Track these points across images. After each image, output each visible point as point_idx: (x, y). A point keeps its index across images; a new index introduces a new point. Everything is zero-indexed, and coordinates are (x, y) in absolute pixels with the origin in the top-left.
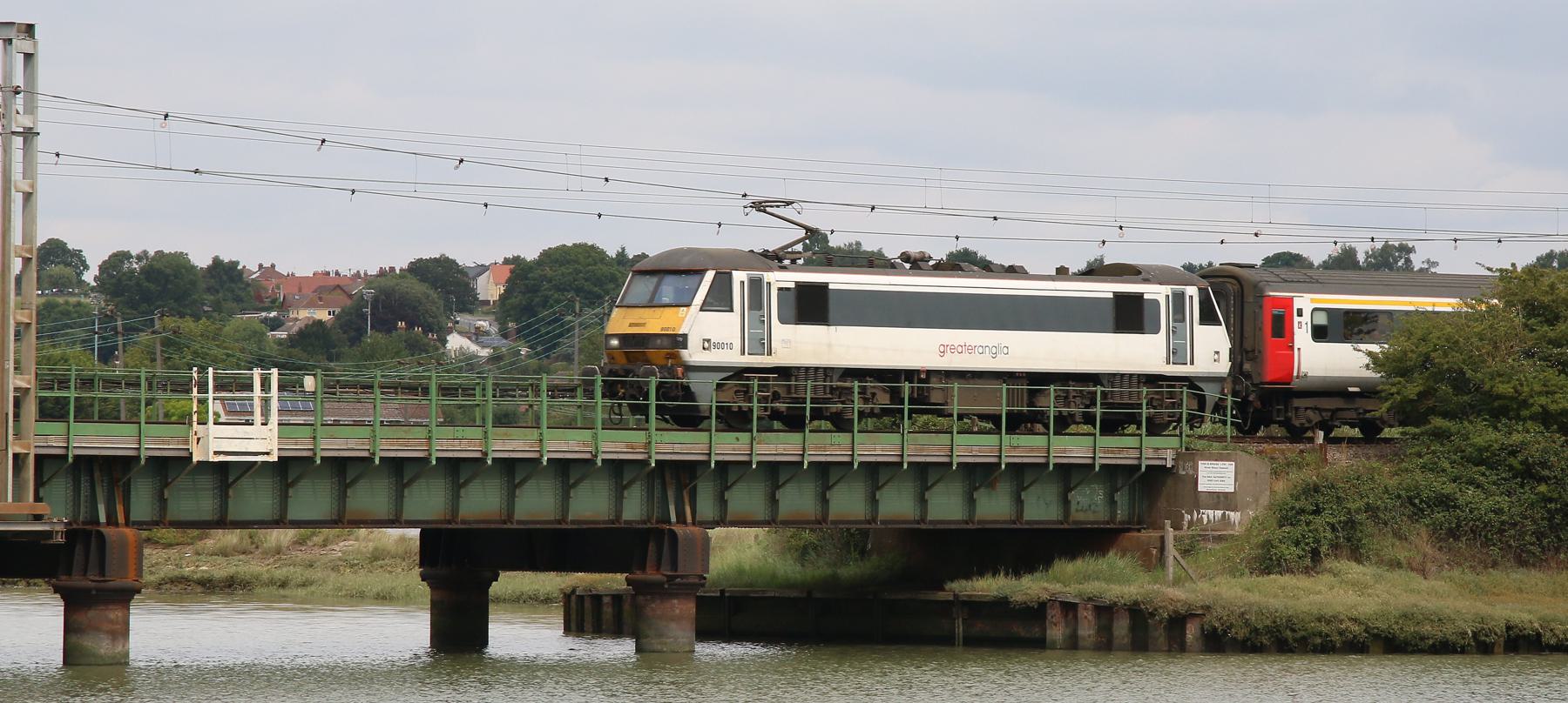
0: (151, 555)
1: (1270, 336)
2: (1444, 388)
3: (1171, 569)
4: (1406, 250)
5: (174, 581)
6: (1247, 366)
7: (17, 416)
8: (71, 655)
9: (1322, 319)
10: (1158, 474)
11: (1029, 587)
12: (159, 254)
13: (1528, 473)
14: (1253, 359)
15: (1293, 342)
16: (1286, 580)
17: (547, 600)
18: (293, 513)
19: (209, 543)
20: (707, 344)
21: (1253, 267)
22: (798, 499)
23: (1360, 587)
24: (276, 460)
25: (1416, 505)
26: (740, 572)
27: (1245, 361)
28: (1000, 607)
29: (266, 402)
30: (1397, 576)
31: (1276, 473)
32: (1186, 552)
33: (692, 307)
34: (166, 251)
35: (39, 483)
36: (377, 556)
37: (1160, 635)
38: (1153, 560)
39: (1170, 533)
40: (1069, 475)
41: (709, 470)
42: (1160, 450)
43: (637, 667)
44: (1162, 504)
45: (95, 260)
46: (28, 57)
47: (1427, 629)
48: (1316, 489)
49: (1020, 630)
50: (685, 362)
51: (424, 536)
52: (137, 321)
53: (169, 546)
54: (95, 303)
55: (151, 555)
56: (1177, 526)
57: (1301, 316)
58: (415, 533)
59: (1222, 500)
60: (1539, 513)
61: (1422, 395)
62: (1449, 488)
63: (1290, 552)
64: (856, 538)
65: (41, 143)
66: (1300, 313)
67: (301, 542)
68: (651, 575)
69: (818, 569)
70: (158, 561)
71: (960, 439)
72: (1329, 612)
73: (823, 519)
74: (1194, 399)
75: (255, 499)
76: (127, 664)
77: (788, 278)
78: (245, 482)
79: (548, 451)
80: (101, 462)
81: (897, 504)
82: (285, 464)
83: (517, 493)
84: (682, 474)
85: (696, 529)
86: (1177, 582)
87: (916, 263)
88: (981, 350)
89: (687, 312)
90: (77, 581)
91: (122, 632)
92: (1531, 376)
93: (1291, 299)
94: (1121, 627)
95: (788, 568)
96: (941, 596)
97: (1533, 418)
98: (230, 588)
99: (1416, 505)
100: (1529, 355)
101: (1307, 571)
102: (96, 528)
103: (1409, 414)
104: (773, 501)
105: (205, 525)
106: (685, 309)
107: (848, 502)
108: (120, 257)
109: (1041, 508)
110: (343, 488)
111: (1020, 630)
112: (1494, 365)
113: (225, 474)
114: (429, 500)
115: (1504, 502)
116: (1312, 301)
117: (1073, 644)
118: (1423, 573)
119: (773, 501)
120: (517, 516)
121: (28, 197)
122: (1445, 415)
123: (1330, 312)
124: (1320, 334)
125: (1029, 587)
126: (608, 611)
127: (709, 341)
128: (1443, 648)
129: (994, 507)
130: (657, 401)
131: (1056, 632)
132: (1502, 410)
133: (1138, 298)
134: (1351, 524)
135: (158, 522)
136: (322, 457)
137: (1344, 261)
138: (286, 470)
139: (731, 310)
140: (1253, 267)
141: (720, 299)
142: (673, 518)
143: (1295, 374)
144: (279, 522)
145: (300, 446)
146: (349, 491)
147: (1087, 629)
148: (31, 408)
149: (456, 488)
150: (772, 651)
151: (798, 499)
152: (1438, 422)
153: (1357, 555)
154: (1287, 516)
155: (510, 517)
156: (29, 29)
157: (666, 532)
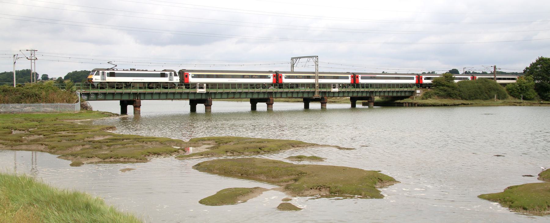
0: (328, 99)
2: (438, 84)
4: (434, 72)
5: (330, 102)
6: (277, 81)
8: (322, 108)
9: (425, 78)
10: (413, 91)
11: (402, 101)
13: (445, 91)
16: (424, 100)
17: (361, 103)
18: (293, 96)
20: (96, 79)
22: (382, 94)
25: (436, 94)
26: (377, 100)
28: (400, 103)
30: (434, 100)
31: (423, 91)
32: (416, 98)
34: (7, 72)
35: (319, 94)
36: (346, 99)
37: (413, 105)
38: (413, 99)
39: (414, 96)
40: (405, 92)
42: (413, 89)
44: (413, 94)
47: (437, 104)
49: (401, 105)
51: (250, 99)
55: (328, 99)
59: (419, 94)
60: (446, 94)
61: (436, 84)
62: (439, 92)
63: (425, 98)
64: (387, 97)
65: (319, 66)
66: (190, 75)
67: (340, 98)
68: (370, 101)
70: (329, 100)
73: (384, 96)
76: (272, 110)
77: (109, 72)
78: (336, 93)
81: (391, 94)
84: (372, 92)
86: (415, 101)
87: (143, 70)
90: (322, 102)
92: (446, 82)
94: (410, 104)
96: (394, 102)
98: (334, 102)
99: (436, 94)
100: (445, 81)
101: (426, 99)
103: (435, 86)
104: (380, 94)
107: (386, 94)
109: (403, 94)
110: (228, 95)
111: (401, 105)
112: (442, 81)
113: (334, 93)
114: (351, 95)
115: (443, 93)
117: (406, 106)
118: (436, 99)
119: (380, 94)
122: (438, 86)
123: (426, 77)
124: (425, 79)
125: (402, 101)
126: (366, 104)
128: (438, 106)
129: (399, 94)
131: (404, 105)
132: (443, 85)
134: (430, 95)
137: (429, 73)
138: (339, 92)
139: (99, 75)
141: (98, 74)
144: (338, 97)
147: (407, 105)
148: (318, 88)
149: (353, 94)
150: (379, 107)
151: (382, 94)
152: (437, 87)
153: (431, 98)
154: (424, 95)
155: (357, 96)
156: (318, 56)
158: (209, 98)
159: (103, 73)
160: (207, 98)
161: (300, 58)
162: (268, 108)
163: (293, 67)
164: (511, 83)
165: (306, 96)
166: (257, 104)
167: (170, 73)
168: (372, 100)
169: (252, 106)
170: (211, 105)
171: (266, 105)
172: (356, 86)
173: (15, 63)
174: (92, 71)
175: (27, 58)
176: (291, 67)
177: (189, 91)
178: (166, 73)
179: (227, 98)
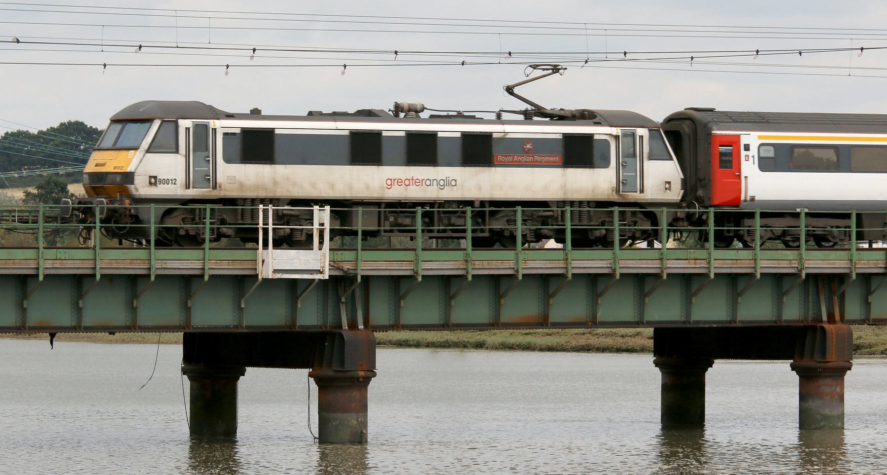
1: (718, 167)
9: (770, 153)
14: (704, 187)
15: (739, 170)
18: (505, 317)
20: (154, 181)
21: (712, 111)
24: (327, 277)
27: (698, 187)
33: (139, 150)
41: (257, 284)
50: (132, 195)
51: (656, 330)
57: (749, 150)
66: (747, 147)
71: (523, 255)
74: (648, 221)
79: (761, 267)
83: (402, 304)
85: (845, 326)
88: (428, 183)
89: (135, 154)
90: (807, 362)
93: (739, 136)
102: (819, 325)
106: (133, 151)
116: (760, 137)
120: (298, 323)
124: (766, 165)
127: (155, 177)
130: (857, 228)
133: (588, 139)
136: (667, 274)
139: (177, 151)
140: (712, 111)
142: (825, 318)
143: (743, 198)
146: (402, 302)
157: (818, 328)
158: (353, 326)
159: (202, 136)
160: (341, 327)
162: (814, 404)
164: (592, 201)
166: (243, 384)
167: (196, 126)
168: (342, 362)
169: (666, 389)
170: (367, 380)
171: (795, 378)
172: (712, 228)
174: (115, 121)
177: (198, 265)
178: (599, 132)
179: (132, 327)
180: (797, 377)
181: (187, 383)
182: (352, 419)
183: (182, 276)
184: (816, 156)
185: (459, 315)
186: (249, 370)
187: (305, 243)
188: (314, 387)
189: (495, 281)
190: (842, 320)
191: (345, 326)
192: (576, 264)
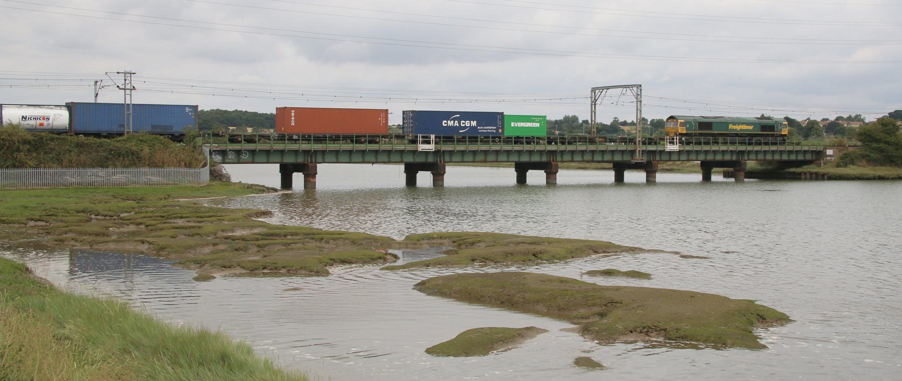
0: (659, 165)
3: (822, 167)
4: (860, 115)
7: (639, 144)
8: (647, 180)
12: (659, 119)
13: (882, 151)
17: (720, 172)
19: (668, 163)
23: (854, 170)
28: (794, 173)
29: (676, 142)
30: (861, 168)
35: (642, 154)
36: (693, 166)
37: (820, 177)
38: (819, 165)
39: (822, 161)
43: (433, 189)
45: (649, 121)
46: (641, 90)
47: (865, 176)
48: (846, 154)
49: (797, 177)
52: (656, 129)
53: (662, 164)
54: (649, 127)
55: (659, 165)
56: (823, 160)
58: (700, 162)
59: (830, 156)
64: (770, 162)
67: (681, 163)
69: (764, 167)
70: (660, 166)
71: (787, 147)
72: (848, 174)
75: (675, 157)
80: (48, 142)
81: (777, 157)
82: (679, 151)
84: (742, 153)
86: (823, 169)
91: (655, 177)
94: (814, 176)
95: (759, 167)
96: (783, 171)
97: (883, 142)
101: (845, 167)
105: (667, 161)
108: (653, 120)
109: (801, 157)
111: (797, 177)
121: (640, 111)
129: (793, 157)
132: (878, 141)
135: (661, 160)
138: (680, 153)
144: (679, 160)
145: (682, 149)
148: (641, 143)
151: (761, 157)
154: (842, 158)
156: (641, 85)
158: (440, 162)
160: (437, 161)
161: (608, 88)
162: (549, 180)
163: (595, 105)
165: (618, 158)
166: (418, 175)
173: (97, 95)
175: (118, 87)
176: (592, 105)
179: (474, 162)
180: (545, 174)
181: (280, 174)
182: (440, 183)
183: (388, 151)
184: (205, 110)
185: (465, 159)
186: (419, 172)
187: (429, 143)
188: (432, 176)
189: (697, 151)
190: (556, 161)
191: (439, 162)
192: (515, 148)
